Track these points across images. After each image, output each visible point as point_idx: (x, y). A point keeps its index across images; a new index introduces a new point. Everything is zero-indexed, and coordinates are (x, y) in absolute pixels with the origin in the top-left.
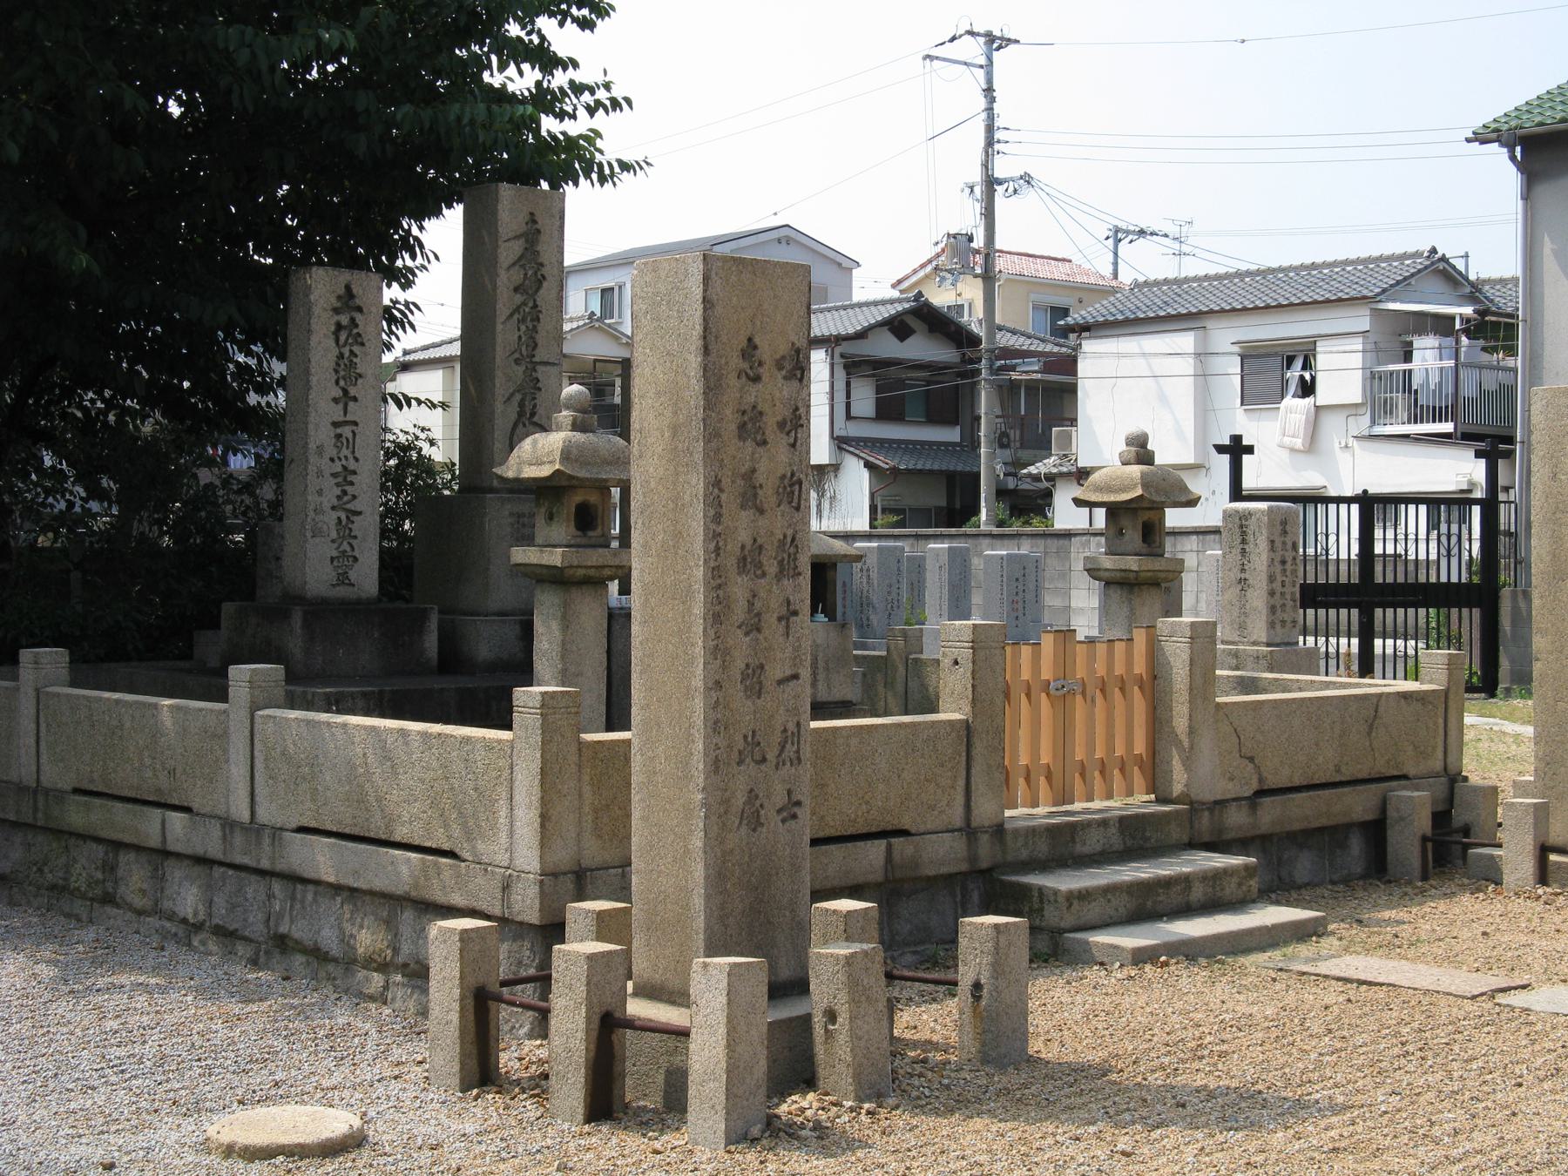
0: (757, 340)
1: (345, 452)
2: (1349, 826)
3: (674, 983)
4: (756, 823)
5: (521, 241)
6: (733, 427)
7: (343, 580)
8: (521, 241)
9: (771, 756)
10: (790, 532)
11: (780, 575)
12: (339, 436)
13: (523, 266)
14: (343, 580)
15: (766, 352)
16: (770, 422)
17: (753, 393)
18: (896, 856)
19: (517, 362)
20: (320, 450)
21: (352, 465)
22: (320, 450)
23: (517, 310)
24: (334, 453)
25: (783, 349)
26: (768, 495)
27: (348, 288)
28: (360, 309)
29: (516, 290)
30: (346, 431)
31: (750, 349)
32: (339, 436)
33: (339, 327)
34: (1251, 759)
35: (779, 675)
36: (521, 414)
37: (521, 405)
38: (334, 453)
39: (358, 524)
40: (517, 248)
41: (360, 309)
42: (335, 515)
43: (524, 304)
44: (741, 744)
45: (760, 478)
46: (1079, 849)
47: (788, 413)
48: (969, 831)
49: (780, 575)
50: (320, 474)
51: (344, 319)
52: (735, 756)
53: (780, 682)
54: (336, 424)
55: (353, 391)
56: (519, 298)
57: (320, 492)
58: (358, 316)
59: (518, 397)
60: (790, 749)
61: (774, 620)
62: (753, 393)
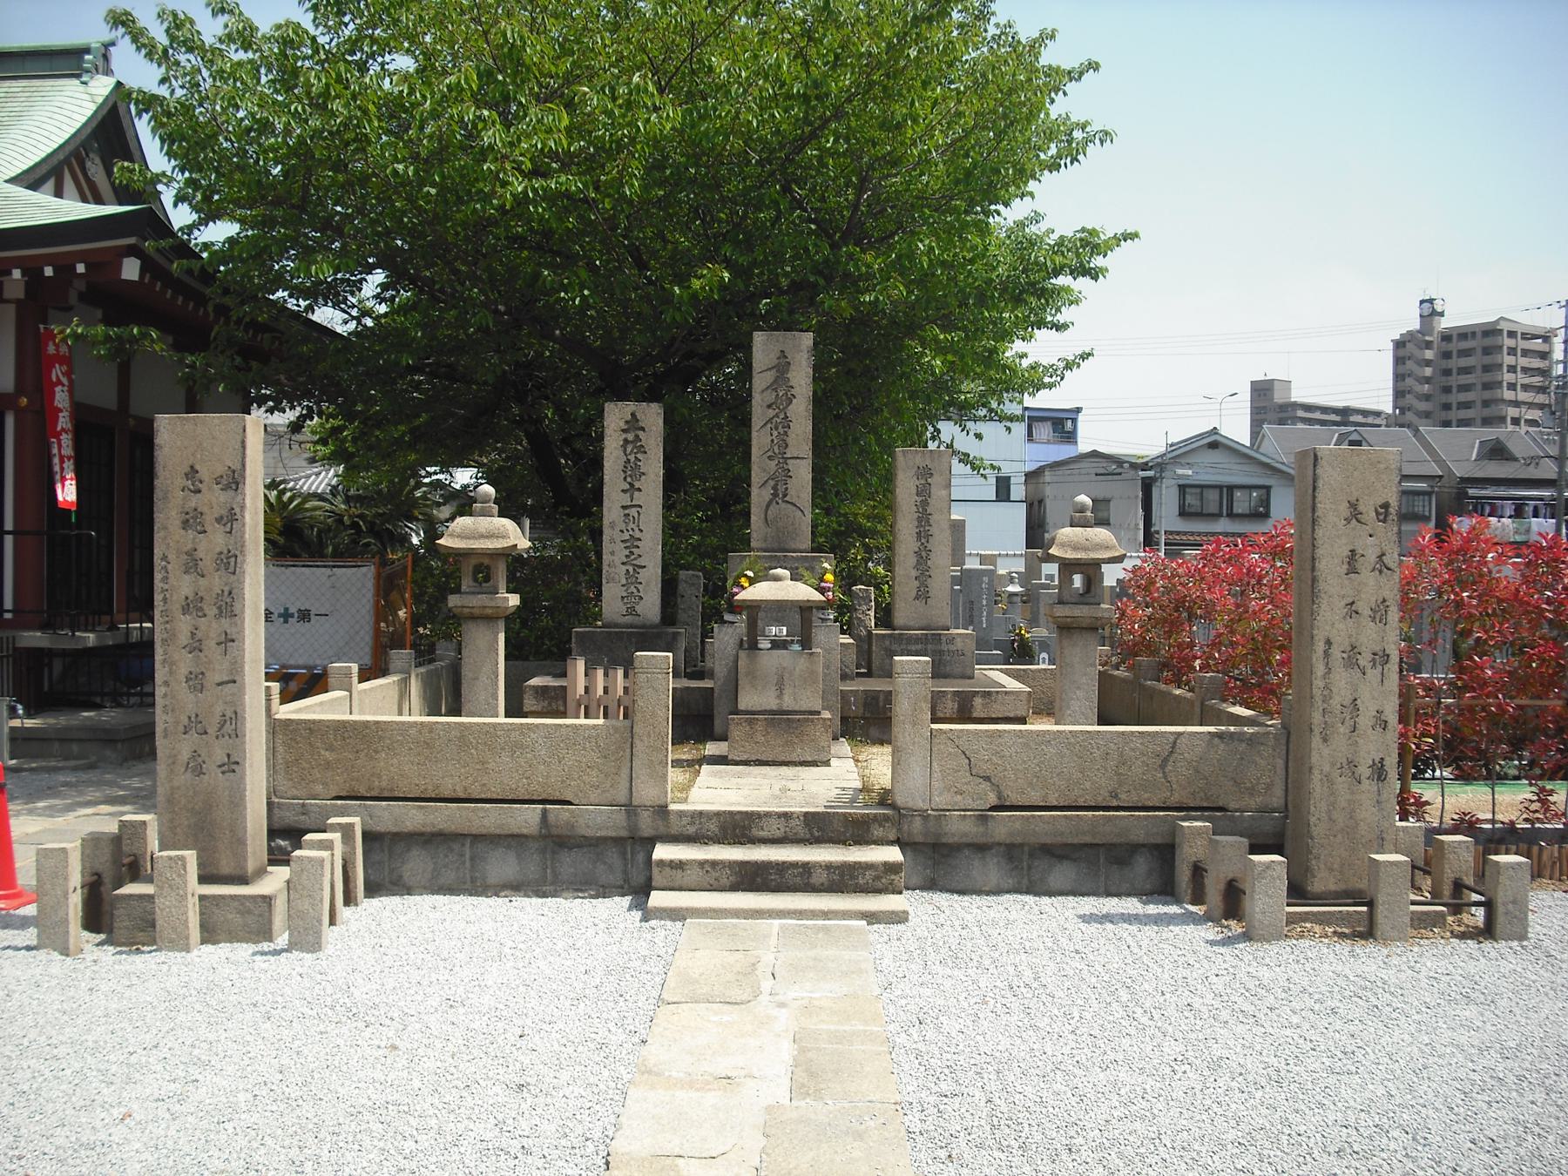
0: (197, 467)
1: (632, 525)
2: (1135, 848)
3: (238, 872)
4: (199, 771)
5: (773, 372)
6: (178, 522)
7: (631, 611)
8: (773, 372)
9: (212, 731)
10: (226, 589)
11: (220, 615)
12: (627, 515)
13: (775, 390)
14: (631, 611)
15: (204, 473)
16: (209, 519)
17: (194, 501)
18: (551, 818)
19: (770, 458)
20: (612, 525)
21: (637, 534)
22: (612, 525)
23: (770, 420)
24: (623, 527)
25: (220, 470)
26: (208, 563)
27: (633, 415)
28: (643, 429)
29: (769, 406)
30: (633, 512)
31: (192, 472)
32: (627, 515)
33: (626, 441)
34: (987, 779)
35: (218, 679)
36: (775, 495)
37: (775, 488)
38: (623, 527)
39: (643, 575)
40: (770, 377)
41: (643, 429)
42: (624, 568)
43: (777, 416)
44: (186, 721)
45: (200, 554)
46: (756, 833)
47: (224, 512)
48: (630, 808)
49: (220, 615)
50: (612, 541)
51: (630, 437)
52: (181, 729)
53: (219, 684)
54: (624, 507)
55: (637, 485)
56: (771, 413)
57: (612, 553)
58: (641, 433)
59: (772, 483)
60: (228, 728)
61: (213, 643)
62: (194, 501)
